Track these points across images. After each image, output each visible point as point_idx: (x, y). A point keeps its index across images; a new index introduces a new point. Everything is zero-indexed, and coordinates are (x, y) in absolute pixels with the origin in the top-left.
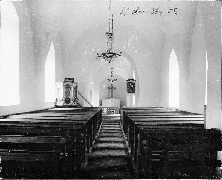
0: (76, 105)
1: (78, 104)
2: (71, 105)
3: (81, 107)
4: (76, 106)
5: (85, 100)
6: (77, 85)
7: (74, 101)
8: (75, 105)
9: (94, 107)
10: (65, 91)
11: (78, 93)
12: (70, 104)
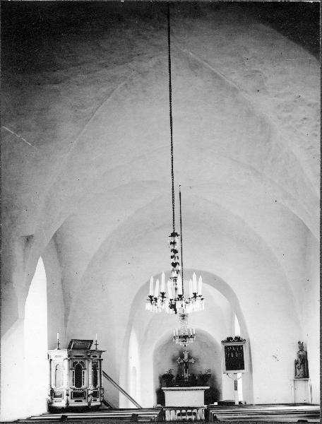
0: (100, 404)
1: (103, 401)
2: (87, 404)
3: (111, 409)
4: (98, 406)
5: (120, 393)
6: (100, 357)
7: (95, 395)
8: (98, 403)
9: (143, 407)
10: (71, 371)
11: (102, 376)
12: (84, 404)
